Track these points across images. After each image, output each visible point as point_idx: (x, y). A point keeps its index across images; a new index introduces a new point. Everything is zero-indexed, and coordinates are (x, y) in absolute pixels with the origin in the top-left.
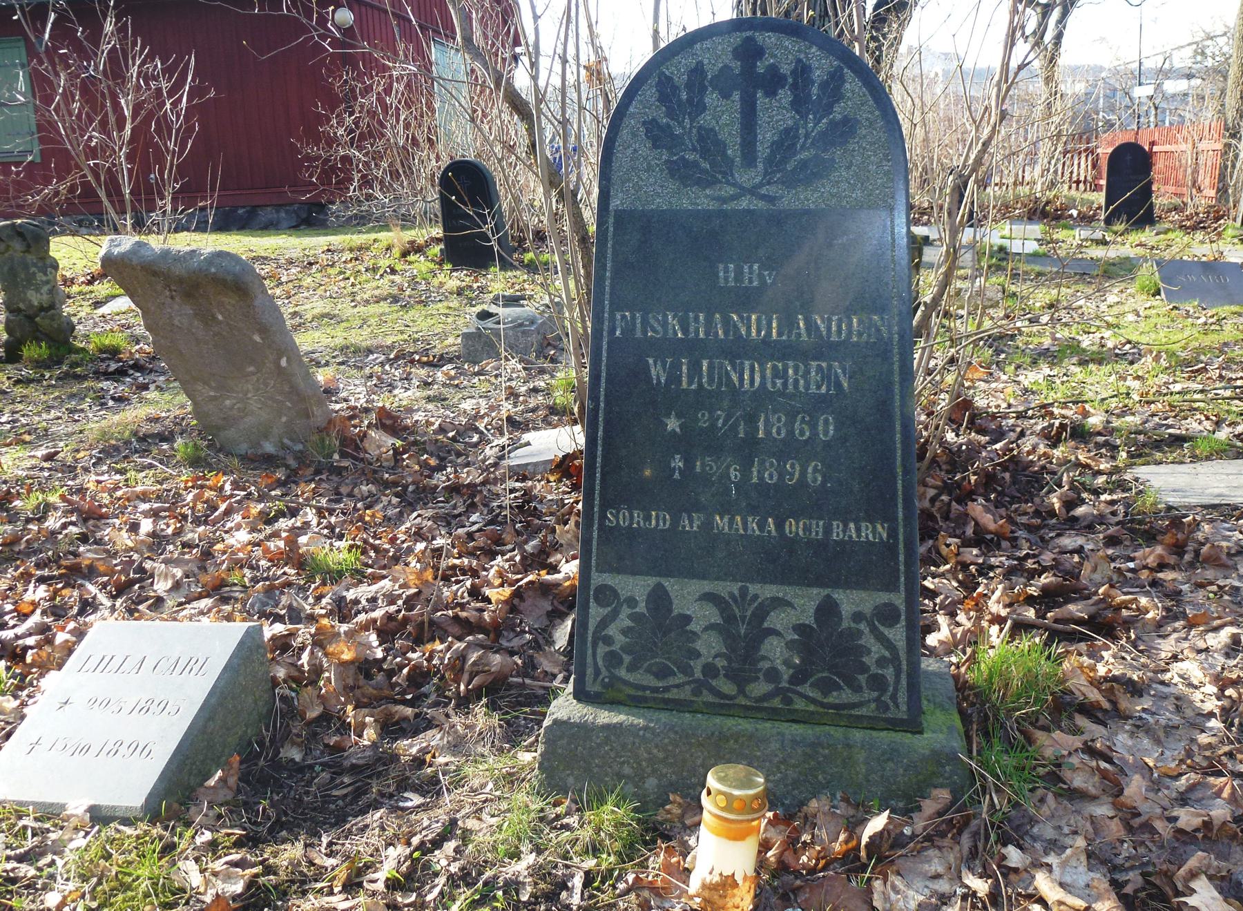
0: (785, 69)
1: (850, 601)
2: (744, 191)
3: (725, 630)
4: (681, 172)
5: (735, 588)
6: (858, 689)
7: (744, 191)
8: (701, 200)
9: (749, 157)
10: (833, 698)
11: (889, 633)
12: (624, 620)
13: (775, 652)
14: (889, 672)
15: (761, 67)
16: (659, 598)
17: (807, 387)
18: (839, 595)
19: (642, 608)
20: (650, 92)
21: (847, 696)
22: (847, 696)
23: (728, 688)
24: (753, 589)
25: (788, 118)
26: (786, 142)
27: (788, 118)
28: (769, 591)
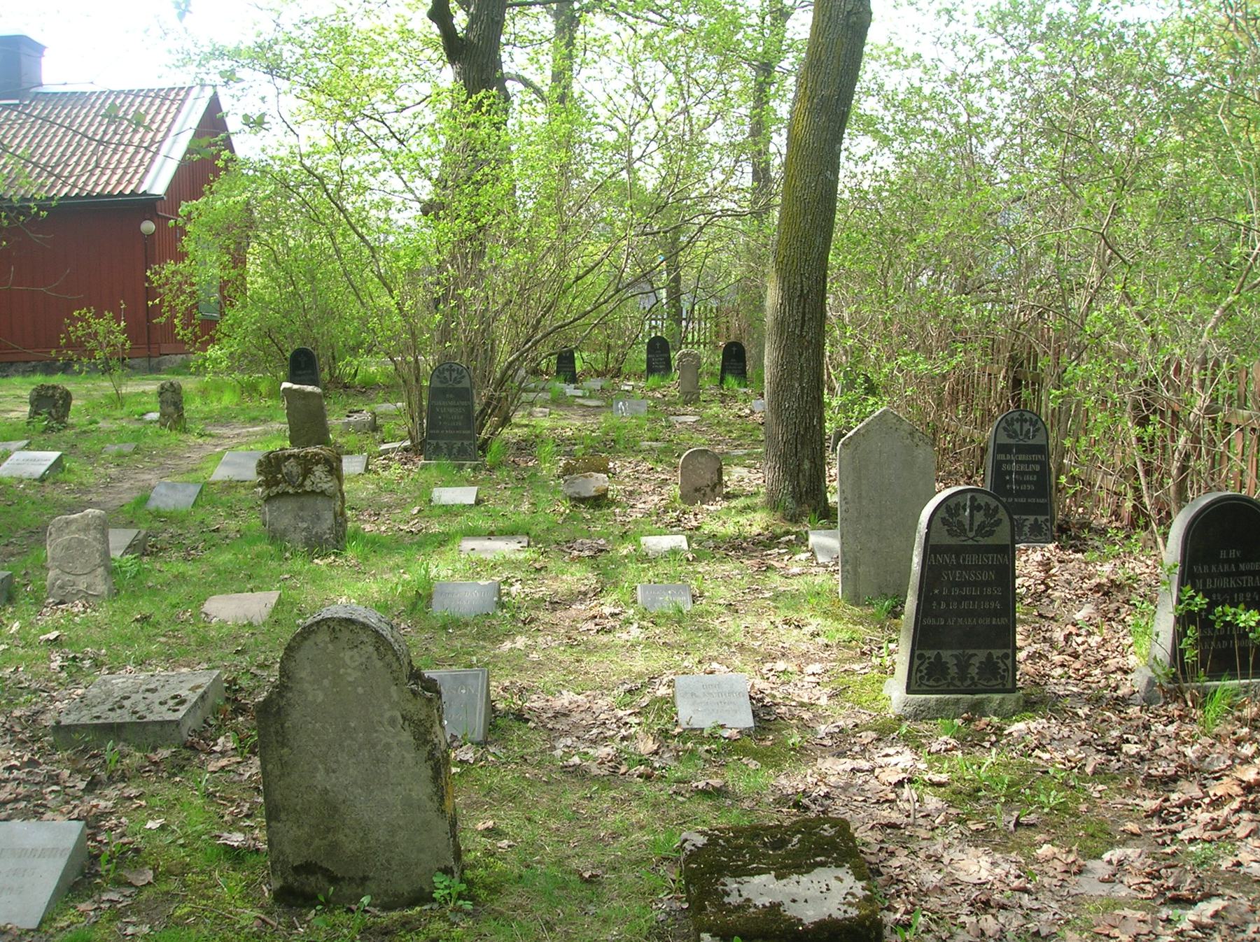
0: (983, 504)
1: (466, 443)
2: (969, 538)
3: (447, 448)
4: (441, 382)
5: (961, 651)
6: (996, 679)
7: (969, 538)
8: (444, 386)
9: (971, 530)
10: (989, 684)
11: (1006, 662)
12: (926, 665)
13: (973, 671)
14: (1006, 674)
15: (976, 504)
16: (437, 444)
17: (954, 579)
18: (993, 651)
19: (932, 660)
20: (943, 508)
21: (994, 682)
22: (994, 682)
23: (958, 683)
24: (967, 651)
25: (983, 519)
26: (982, 526)
27: (983, 519)
28: (971, 652)
